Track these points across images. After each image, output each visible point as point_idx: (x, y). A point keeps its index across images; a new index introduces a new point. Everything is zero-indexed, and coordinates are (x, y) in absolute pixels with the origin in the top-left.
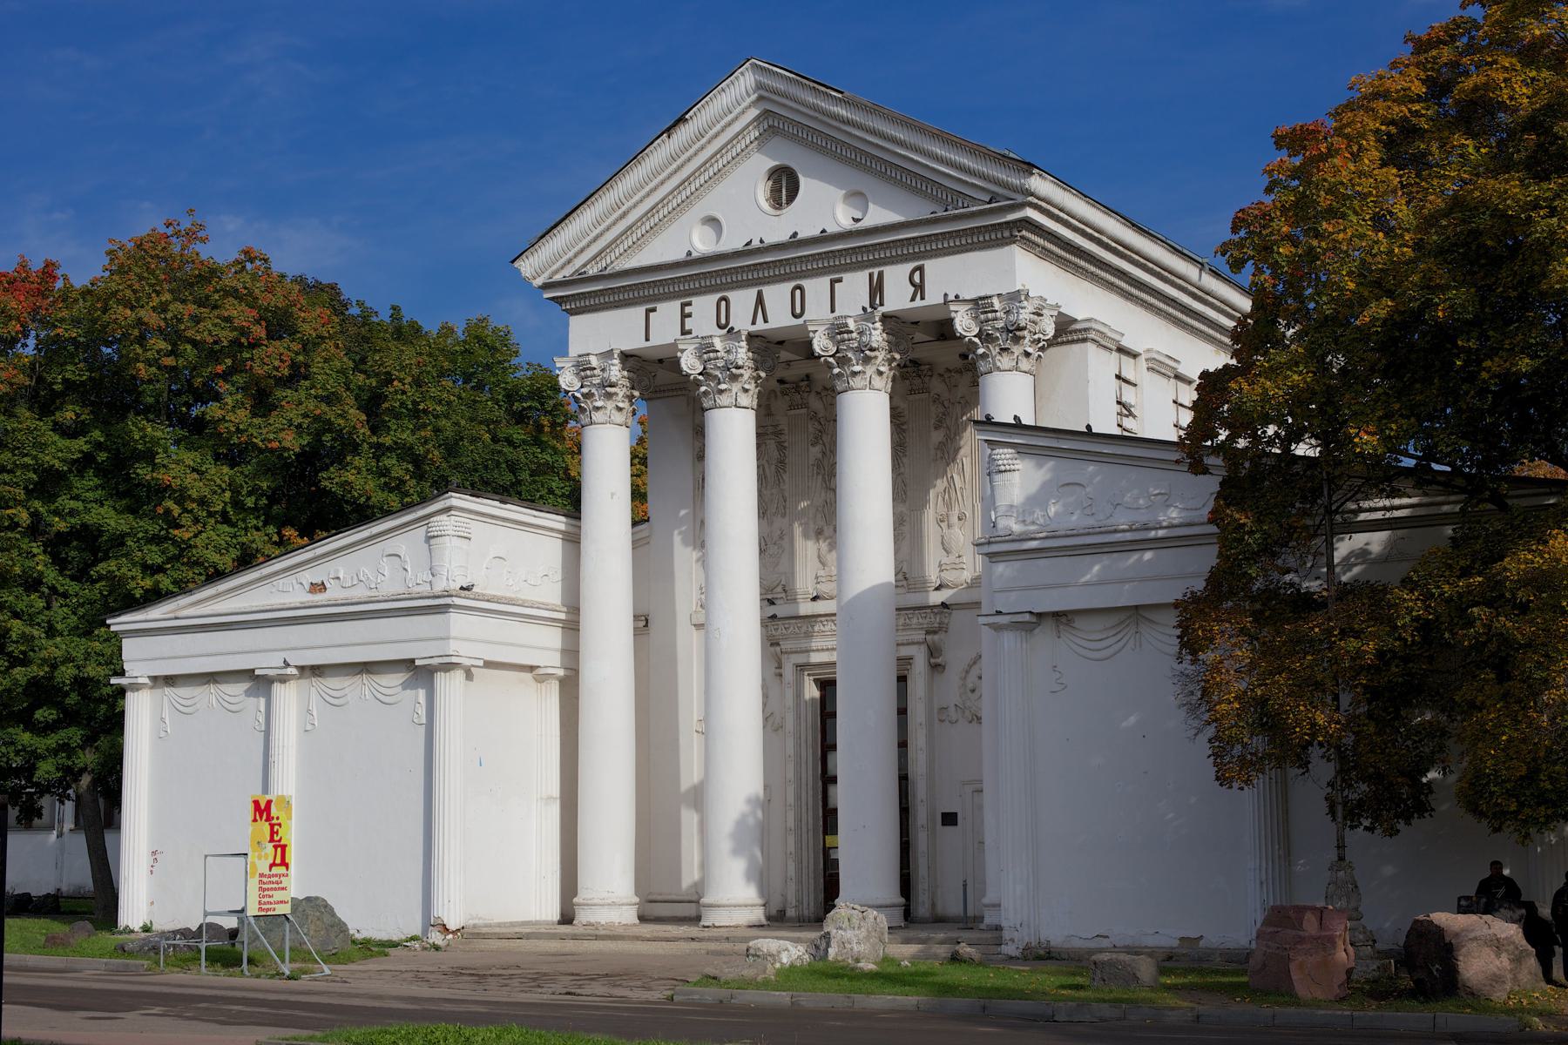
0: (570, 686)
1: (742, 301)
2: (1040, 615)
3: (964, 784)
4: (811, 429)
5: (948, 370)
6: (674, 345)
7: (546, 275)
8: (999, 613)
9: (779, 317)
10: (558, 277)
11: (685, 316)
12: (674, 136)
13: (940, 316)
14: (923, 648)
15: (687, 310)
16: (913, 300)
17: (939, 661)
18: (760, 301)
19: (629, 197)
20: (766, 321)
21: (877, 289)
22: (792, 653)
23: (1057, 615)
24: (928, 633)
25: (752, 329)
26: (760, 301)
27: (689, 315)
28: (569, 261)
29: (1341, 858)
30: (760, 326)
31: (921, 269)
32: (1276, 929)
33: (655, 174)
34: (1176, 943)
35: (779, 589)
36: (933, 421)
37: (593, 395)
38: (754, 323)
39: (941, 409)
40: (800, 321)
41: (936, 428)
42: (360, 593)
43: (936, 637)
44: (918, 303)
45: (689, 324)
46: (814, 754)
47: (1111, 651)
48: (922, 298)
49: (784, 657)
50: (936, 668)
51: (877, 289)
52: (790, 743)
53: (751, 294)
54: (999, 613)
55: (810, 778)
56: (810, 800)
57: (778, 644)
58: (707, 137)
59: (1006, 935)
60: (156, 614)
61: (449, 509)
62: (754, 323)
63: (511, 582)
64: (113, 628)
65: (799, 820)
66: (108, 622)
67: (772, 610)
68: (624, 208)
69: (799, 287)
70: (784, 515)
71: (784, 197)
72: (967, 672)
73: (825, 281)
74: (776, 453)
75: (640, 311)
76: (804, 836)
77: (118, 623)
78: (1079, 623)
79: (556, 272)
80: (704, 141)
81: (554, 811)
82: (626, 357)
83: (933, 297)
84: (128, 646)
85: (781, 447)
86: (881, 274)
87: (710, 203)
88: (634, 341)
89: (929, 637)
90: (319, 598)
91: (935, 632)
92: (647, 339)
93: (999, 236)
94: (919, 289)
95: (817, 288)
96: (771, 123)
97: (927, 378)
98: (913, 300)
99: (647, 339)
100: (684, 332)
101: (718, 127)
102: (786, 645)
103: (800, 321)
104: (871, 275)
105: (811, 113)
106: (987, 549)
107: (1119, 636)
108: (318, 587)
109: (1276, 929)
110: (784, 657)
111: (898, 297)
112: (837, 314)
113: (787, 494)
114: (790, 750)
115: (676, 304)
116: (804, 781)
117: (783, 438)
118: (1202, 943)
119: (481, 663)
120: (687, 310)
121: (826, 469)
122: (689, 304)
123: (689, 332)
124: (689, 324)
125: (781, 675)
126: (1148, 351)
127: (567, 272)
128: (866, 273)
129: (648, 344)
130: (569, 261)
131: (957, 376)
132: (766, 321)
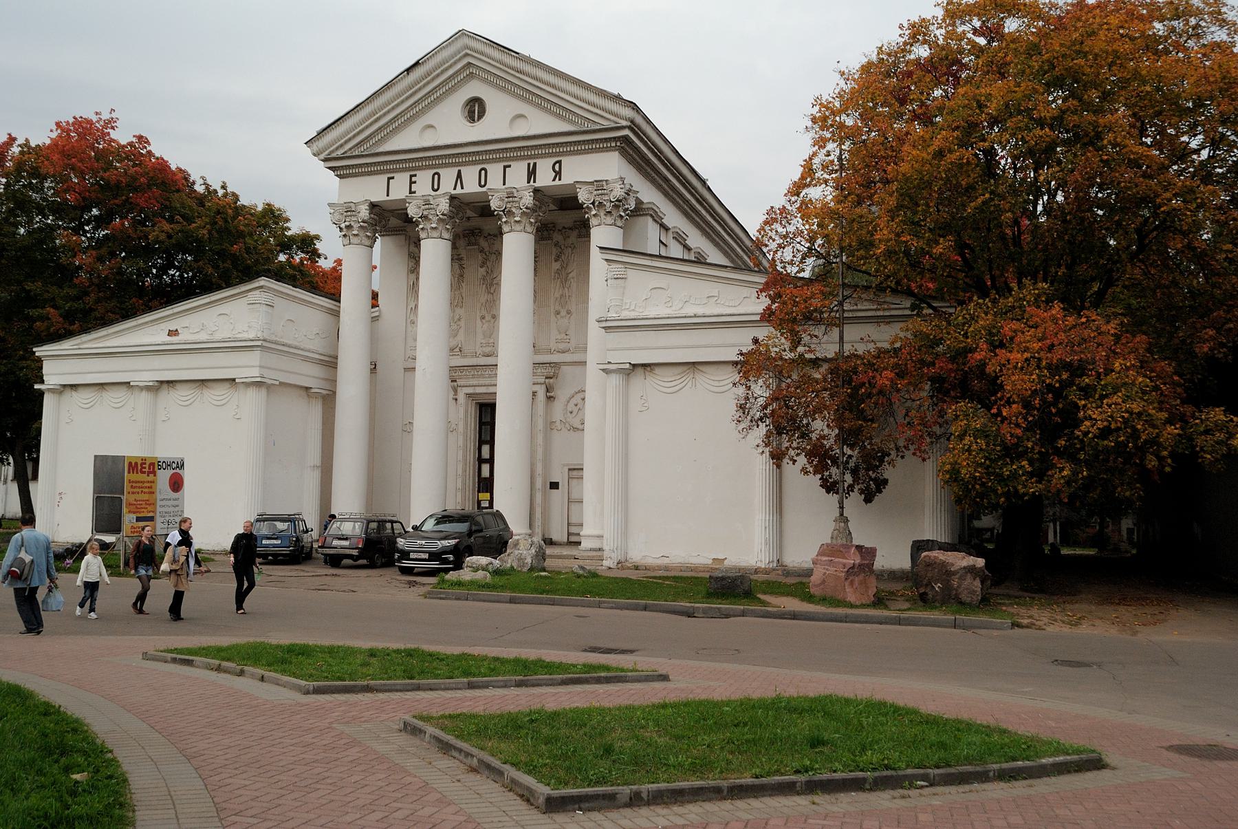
0: (329, 399)
1: (448, 176)
2: (634, 366)
3: (564, 465)
4: (480, 258)
5: (564, 228)
6: (404, 201)
7: (327, 152)
8: (609, 363)
9: (471, 186)
10: (334, 155)
11: (411, 183)
12: (411, 74)
13: (567, 193)
14: (544, 387)
15: (414, 179)
16: (554, 180)
17: (552, 394)
18: (459, 175)
19: (381, 108)
20: (462, 188)
21: (532, 173)
22: (463, 386)
23: (644, 366)
24: (547, 378)
25: (454, 192)
26: (459, 175)
27: (415, 182)
28: (341, 146)
29: (842, 514)
30: (459, 191)
31: (560, 162)
32: (830, 559)
33: (399, 95)
34: (710, 562)
35: (457, 350)
36: (553, 257)
37: (352, 227)
38: (455, 189)
39: (560, 250)
40: (484, 189)
41: (556, 261)
42: (203, 336)
43: (551, 380)
44: (557, 182)
45: (414, 187)
46: (475, 445)
47: (677, 388)
48: (560, 179)
49: (459, 389)
50: (550, 398)
51: (532, 173)
52: (461, 438)
53: (454, 171)
54: (609, 363)
55: (472, 460)
56: (471, 472)
57: (455, 381)
58: (432, 76)
59: (606, 554)
60: (66, 346)
61: (261, 287)
62: (455, 189)
63: (296, 336)
64: (37, 354)
65: (464, 484)
66: (34, 350)
67: (458, 361)
68: (377, 116)
69: (485, 170)
70: (461, 307)
71: (476, 116)
72: (568, 402)
73: (500, 166)
74: (458, 270)
75: (384, 178)
76: (467, 493)
77: (39, 351)
78: (657, 370)
79: (333, 152)
80: (429, 78)
81: (317, 474)
82: (373, 206)
83: (567, 179)
84: (47, 368)
85: (462, 267)
86: (535, 164)
87: (429, 118)
88: (379, 196)
89: (547, 380)
90: (174, 339)
91: (551, 378)
92: (388, 195)
93: (609, 145)
94: (558, 174)
95: (495, 170)
96: (471, 71)
97: (552, 232)
98: (554, 180)
99: (388, 195)
100: (411, 192)
101: (439, 71)
102: (460, 382)
103: (484, 189)
104: (529, 164)
105: (498, 65)
106: (604, 324)
107: (683, 379)
108: (173, 333)
109: (830, 559)
110: (459, 389)
111: (545, 178)
112: (506, 186)
113: (464, 296)
114: (461, 443)
115: (407, 175)
116: (468, 461)
117: (463, 262)
118: (726, 562)
119: (277, 383)
120: (414, 179)
121: (492, 282)
122: (415, 175)
123: (415, 192)
124: (414, 187)
125: (456, 400)
126: (674, 227)
127: (340, 152)
128: (526, 163)
129: (388, 198)
130: (341, 146)
131: (571, 231)
132: (462, 188)
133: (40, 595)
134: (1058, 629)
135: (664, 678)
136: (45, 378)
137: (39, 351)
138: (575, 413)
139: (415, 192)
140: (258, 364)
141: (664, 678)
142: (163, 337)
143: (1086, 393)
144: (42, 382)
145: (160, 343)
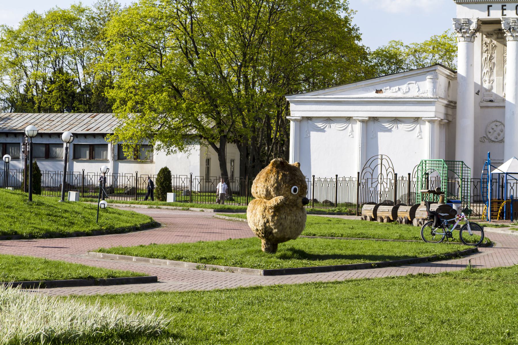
27: (505, 9)
77: (288, 98)
92: (488, 16)
120: (504, 8)
122: (505, 6)
123: (505, 15)
129: (489, 17)
133: (261, 218)
134: (369, 232)
135: (154, 280)
136: (291, 113)
137: (288, 98)
138: (491, 133)
139: (505, 15)
140: (434, 110)
141: (154, 280)
142: (373, 94)
143: (88, 91)
144: (290, 115)
145: (373, 97)
